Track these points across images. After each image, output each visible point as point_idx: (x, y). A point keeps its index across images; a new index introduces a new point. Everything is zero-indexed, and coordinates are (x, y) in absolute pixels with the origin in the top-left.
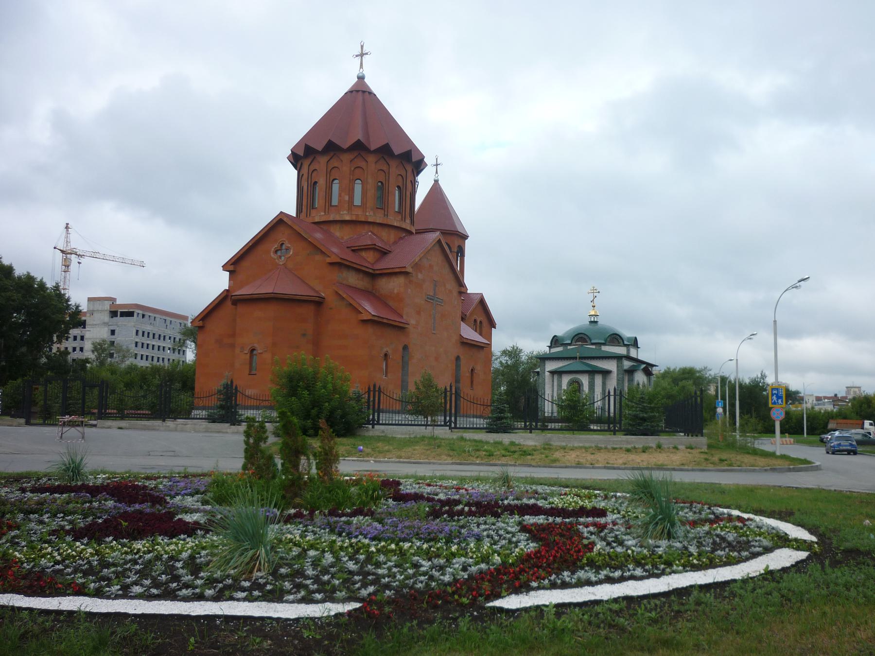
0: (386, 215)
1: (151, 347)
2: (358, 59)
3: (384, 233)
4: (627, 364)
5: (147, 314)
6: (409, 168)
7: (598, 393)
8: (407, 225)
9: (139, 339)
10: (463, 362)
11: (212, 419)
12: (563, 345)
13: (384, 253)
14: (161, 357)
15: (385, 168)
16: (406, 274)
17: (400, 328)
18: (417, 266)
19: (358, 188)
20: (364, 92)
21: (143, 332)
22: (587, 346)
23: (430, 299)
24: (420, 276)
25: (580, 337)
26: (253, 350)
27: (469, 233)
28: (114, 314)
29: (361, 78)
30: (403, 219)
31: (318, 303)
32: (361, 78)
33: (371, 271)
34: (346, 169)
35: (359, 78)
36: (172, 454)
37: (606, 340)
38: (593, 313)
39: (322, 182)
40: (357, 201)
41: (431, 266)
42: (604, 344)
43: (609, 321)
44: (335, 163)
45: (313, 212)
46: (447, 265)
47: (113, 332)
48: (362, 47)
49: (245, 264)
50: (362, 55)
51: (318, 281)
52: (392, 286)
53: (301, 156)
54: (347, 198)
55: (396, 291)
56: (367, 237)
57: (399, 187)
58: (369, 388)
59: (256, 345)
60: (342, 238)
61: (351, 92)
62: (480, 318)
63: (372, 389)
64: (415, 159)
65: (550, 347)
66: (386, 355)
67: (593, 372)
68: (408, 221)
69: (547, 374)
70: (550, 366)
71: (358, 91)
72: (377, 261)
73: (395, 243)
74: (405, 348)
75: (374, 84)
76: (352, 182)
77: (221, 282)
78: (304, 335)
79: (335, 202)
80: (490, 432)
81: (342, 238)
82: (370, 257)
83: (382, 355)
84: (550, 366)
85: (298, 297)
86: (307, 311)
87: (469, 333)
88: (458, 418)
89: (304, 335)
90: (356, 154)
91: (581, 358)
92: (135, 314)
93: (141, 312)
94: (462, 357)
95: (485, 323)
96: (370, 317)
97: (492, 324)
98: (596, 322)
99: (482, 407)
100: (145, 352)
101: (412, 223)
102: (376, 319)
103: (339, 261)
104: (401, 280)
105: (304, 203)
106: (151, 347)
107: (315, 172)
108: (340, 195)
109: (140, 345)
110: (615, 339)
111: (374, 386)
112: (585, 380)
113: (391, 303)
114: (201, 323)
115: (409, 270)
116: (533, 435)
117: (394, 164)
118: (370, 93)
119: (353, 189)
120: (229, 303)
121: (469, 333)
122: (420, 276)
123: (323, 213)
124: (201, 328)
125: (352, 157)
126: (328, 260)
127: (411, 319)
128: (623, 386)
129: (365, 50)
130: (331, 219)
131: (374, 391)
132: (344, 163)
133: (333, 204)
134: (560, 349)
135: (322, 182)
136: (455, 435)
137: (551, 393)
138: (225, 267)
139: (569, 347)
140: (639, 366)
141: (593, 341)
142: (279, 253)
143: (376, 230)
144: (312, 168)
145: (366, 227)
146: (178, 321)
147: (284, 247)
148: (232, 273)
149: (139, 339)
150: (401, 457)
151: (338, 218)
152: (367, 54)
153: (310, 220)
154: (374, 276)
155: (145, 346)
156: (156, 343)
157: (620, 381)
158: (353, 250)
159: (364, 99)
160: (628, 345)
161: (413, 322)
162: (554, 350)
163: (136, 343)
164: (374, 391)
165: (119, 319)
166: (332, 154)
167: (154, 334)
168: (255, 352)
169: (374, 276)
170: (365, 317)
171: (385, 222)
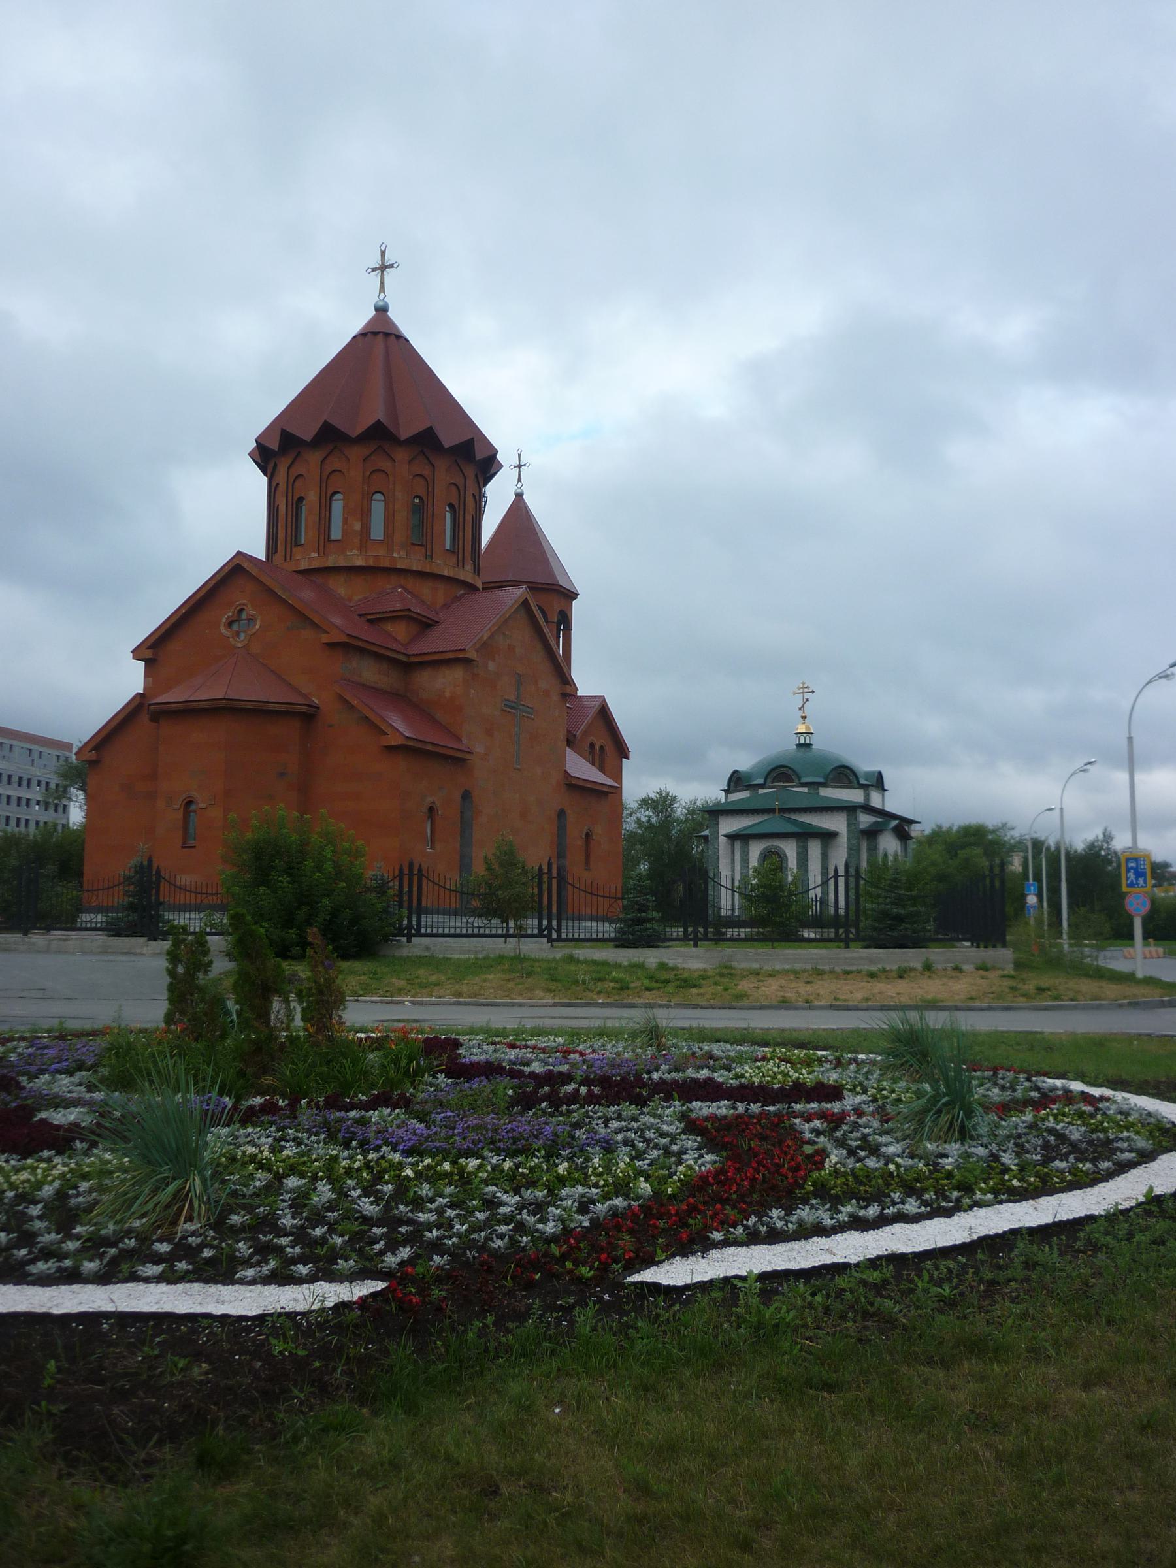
0: (429, 556)
2: (376, 277)
3: (425, 590)
4: (865, 820)
6: (470, 471)
11: (113, 929)
13: (425, 625)
15: (427, 472)
16: (467, 662)
17: (457, 761)
18: (486, 648)
19: (378, 508)
20: (387, 335)
22: (797, 787)
24: (491, 666)
25: (780, 773)
29: (382, 310)
30: (461, 564)
31: (308, 717)
32: (382, 310)
33: (402, 658)
35: (377, 309)
39: (312, 497)
40: (377, 532)
42: (824, 785)
44: (335, 463)
48: (383, 253)
50: (383, 268)
52: (443, 683)
55: (447, 694)
56: (395, 596)
57: (451, 506)
58: (401, 870)
59: (195, 794)
61: (363, 335)
64: (480, 455)
67: (805, 835)
68: (469, 567)
69: (722, 840)
70: (728, 826)
71: (375, 334)
73: (446, 606)
76: (368, 497)
77: (131, 679)
79: (336, 534)
82: (400, 631)
83: (425, 809)
84: (728, 826)
85: (271, 707)
87: (580, 768)
88: (564, 923)
91: (782, 810)
95: (610, 750)
97: (622, 751)
98: (809, 745)
105: (281, 535)
106: (14, 801)
108: (345, 521)
110: (844, 775)
111: (411, 865)
112: (790, 849)
114: (93, 755)
115: (472, 654)
117: (441, 464)
118: (399, 337)
119: (369, 511)
120: (144, 718)
121: (580, 768)
122: (491, 666)
123: (314, 555)
124: (93, 763)
126: (325, 638)
127: (476, 743)
130: (330, 564)
131: (411, 874)
133: (333, 537)
135: (312, 497)
138: (137, 653)
139: (761, 791)
141: (804, 780)
142: (235, 627)
146: (54, 752)
147: (244, 616)
148: (150, 663)
150: (460, 995)
154: (408, 666)
157: (853, 851)
158: (369, 621)
160: (867, 786)
161: (479, 749)
162: (734, 797)
164: (411, 874)
167: (10, 777)
168: (193, 807)
169: (408, 666)
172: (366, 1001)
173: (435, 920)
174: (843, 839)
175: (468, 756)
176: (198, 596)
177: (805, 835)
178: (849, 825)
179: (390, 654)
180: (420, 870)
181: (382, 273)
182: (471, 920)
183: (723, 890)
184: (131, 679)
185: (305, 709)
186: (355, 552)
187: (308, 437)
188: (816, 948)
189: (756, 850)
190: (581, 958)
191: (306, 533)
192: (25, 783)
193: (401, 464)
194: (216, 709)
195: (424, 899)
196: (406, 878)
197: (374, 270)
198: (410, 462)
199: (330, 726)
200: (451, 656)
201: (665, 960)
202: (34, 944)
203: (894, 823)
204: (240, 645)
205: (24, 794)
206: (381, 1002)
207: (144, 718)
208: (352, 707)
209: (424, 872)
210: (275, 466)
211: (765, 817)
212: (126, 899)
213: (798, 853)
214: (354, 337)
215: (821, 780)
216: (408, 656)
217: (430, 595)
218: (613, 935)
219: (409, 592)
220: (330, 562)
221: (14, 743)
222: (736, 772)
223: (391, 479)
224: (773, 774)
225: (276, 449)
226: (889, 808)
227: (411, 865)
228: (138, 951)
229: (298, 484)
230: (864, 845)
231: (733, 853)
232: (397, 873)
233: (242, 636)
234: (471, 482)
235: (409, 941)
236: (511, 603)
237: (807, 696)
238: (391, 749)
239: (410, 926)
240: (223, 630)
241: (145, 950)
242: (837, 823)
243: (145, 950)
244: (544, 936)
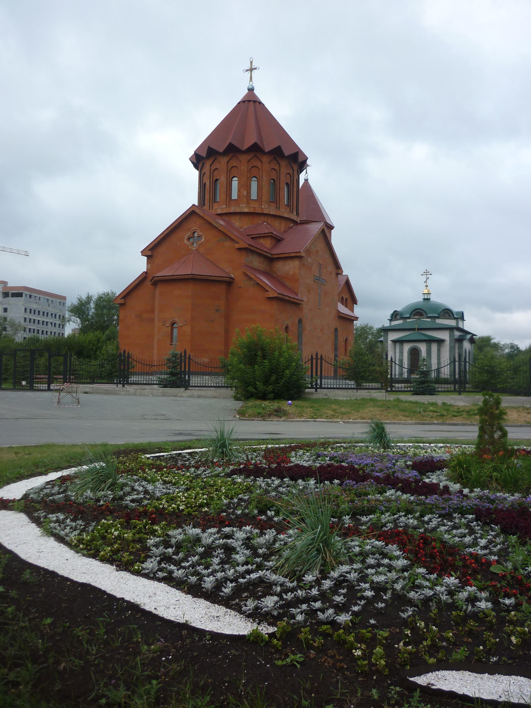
0: (278, 208)
1: (36, 322)
2: (248, 74)
3: (276, 223)
4: (457, 334)
5: (33, 294)
6: (296, 168)
7: (440, 360)
8: (294, 217)
9: (28, 316)
10: (340, 332)
11: (165, 384)
12: (402, 318)
13: (278, 240)
14: (45, 330)
16: (300, 257)
17: (296, 304)
18: (308, 251)
19: (254, 185)
20: (255, 102)
21: (31, 310)
22: (425, 319)
23: (317, 279)
24: (310, 260)
25: (417, 311)
26: (174, 323)
27: (335, 226)
28: (6, 295)
30: (291, 211)
31: (229, 283)
33: (270, 255)
34: (244, 168)
35: (249, 90)
36: (163, 417)
37: (439, 314)
38: (426, 292)
39: (223, 179)
40: (254, 196)
41: (317, 251)
42: (438, 318)
43: (441, 297)
44: (234, 163)
45: (216, 206)
46: (328, 251)
47: (5, 310)
48: (251, 62)
49: (161, 249)
50: (251, 70)
51: (226, 263)
52: (289, 268)
54: (245, 193)
55: (291, 273)
56: (264, 227)
57: (287, 184)
58: (312, 356)
59: (176, 319)
60: (242, 228)
61: (243, 102)
62: (346, 296)
63: (314, 357)
64: (300, 160)
65: (391, 320)
66: (287, 327)
67: (430, 341)
68: (295, 213)
69: (390, 342)
70: (393, 336)
71: (249, 101)
72: (274, 247)
73: (285, 231)
74: (300, 321)
75: (261, 95)
76: (249, 180)
77: (141, 265)
78: (217, 310)
79: (235, 196)
80: (417, 394)
81: (242, 228)
82: (267, 243)
83: (284, 328)
84: (393, 336)
85: (212, 278)
86: (220, 290)
87: (343, 309)
88: (323, 380)
90: (252, 155)
91: (419, 329)
92: (24, 295)
93: (28, 293)
94: (339, 329)
95: (349, 301)
96: (275, 295)
97: (354, 301)
98: (429, 299)
99: (148, 366)
101: (298, 214)
102: (280, 296)
103: (247, 246)
104: (296, 263)
105: (207, 197)
106: (36, 322)
107: (217, 171)
108: (239, 191)
109: (28, 320)
110: (447, 313)
111: (317, 354)
112: (423, 347)
113: (287, 283)
114: (122, 301)
115: (303, 254)
116: (463, 396)
117: (283, 163)
118: (260, 103)
119: (250, 185)
120: (148, 283)
121: (343, 309)
122: (310, 260)
123: (224, 206)
124: (122, 305)
125: (228, 158)
126: (237, 246)
127: (303, 296)
128: (454, 353)
129: (254, 65)
130: (232, 211)
131: (317, 359)
132: (243, 163)
133: (233, 198)
134: (400, 322)
135: (223, 179)
136: (392, 397)
137: (398, 357)
138: (143, 253)
139: (408, 320)
140: (466, 336)
141: (429, 315)
142: (191, 240)
143: (270, 220)
145: (262, 218)
146: (58, 301)
147: (196, 235)
148: (149, 257)
149: (28, 316)
150: (364, 418)
152: (256, 69)
153: (213, 212)
154: (271, 260)
155: (32, 321)
156: (41, 318)
157: (452, 349)
158: (252, 238)
159: (255, 108)
160: (457, 318)
161: (305, 299)
162: (394, 323)
163: (25, 318)
164: (317, 359)
165: (10, 299)
166: (232, 155)
167: (39, 312)
168: (175, 326)
169: (271, 260)
170: (271, 295)
171: (277, 214)
172: (320, 421)
173: (196, 379)
174: (447, 343)
175: (302, 303)
176: (173, 226)
177: (430, 341)
178: (450, 336)
179: (265, 253)
180: (321, 357)
181: (251, 72)
182: (150, 377)
183: (406, 367)
184: (141, 265)
185: (228, 279)
186: (244, 205)
187: (221, 151)
188: (454, 394)
189: (407, 347)
190: (403, 400)
191: (220, 195)
192: (45, 314)
193: (266, 164)
194: (205, 280)
195: (191, 368)
196: (314, 361)
197: (247, 71)
198: (269, 162)
199: (240, 288)
200: (293, 255)
201: (445, 401)
202: (128, 391)
203: (469, 336)
204: (194, 249)
205: (45, 319)
206: (327, 422)
207: (148, 283)
208: (251, 278)
209: (324, 358)
210: (203, 164)
211: (410, 332)
212: (168, 370)
213: (427, 349)
214: (239, 103)
215: (437, 315)
216: (272, 255)
217: (278, 227)
218: (157, 382)
219: (269, 225)
221: (41, 296)
222: (395, 311)
223: (261, 170)
224: (414, 312)
225: (205, 156)
226: (466, 328)
227: (317, 354)
228: (180, 395)
229: (215, 173)
230: (457, 345)
231: (395, 349)
232: (310, 358)
233: (195, 245)
234: (295, 173)
235: (316, 391)
236: (317, 230)
237: (428, 276)
238: (270, 299)
239: (316, 384)
240: (186, 241)
241: (184, 394)
242: (445, 336)
243: (184, 394)
244: (314, 388)
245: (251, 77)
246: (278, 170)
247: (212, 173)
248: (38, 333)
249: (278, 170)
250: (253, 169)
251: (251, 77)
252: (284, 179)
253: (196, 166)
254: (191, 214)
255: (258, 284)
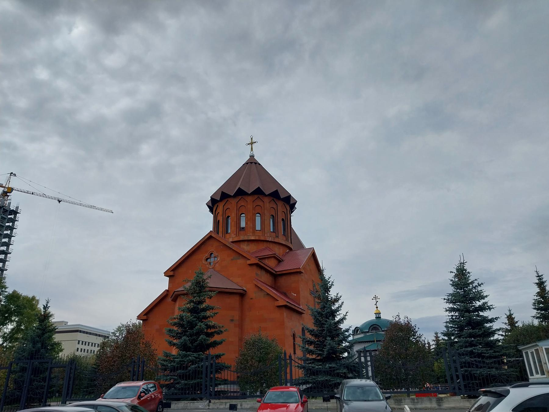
2: (250, 146)
6: (288, 208)
12: (363, 332)
13: (279, 261)
15: (275, 206)
19: (258, 219)
20: (256, 163)
29: (252, 157)
31: (242, 295)
32: (252, 157)
33: (274, 272)
35: (250, 156)
40: (258, 227)
44: (242, 203)
48: (252, 139)
49: (181, 270)
50: (252, 143)
53: (213, 204)
61: (247, 163)
71: (251, 163)
86: (234, 301)
89: (232, 320)
100: (83, 347)
107: (228, 210)
118: (259, 164)
120: (169, 300)
126: (249, 262)
130: (241, 239)
134: (362, 335)
135: (233, 215)
138: (166, 274)
139: (368, 334)
144: (225, 208)
147: (213, 255)
151: (246, 238)
158: (259, 259)
166: (240, 197)
192: (83, 351)
193: (267, 203)
197: (248, 144)
207: (169, 300)
211: (371, 344)
220: (242, 238)
224: (372, 328)
240: (204, 262)
245: (252, 149)
246: (276, 209)
247: (224, 212)
248: (87, 352)
249: (276, 209)
250: (257, 207)
251: (252, 149)
252: (281, 216)
253: (211, 210)
254: (209, 238)
255: (268, 294)
